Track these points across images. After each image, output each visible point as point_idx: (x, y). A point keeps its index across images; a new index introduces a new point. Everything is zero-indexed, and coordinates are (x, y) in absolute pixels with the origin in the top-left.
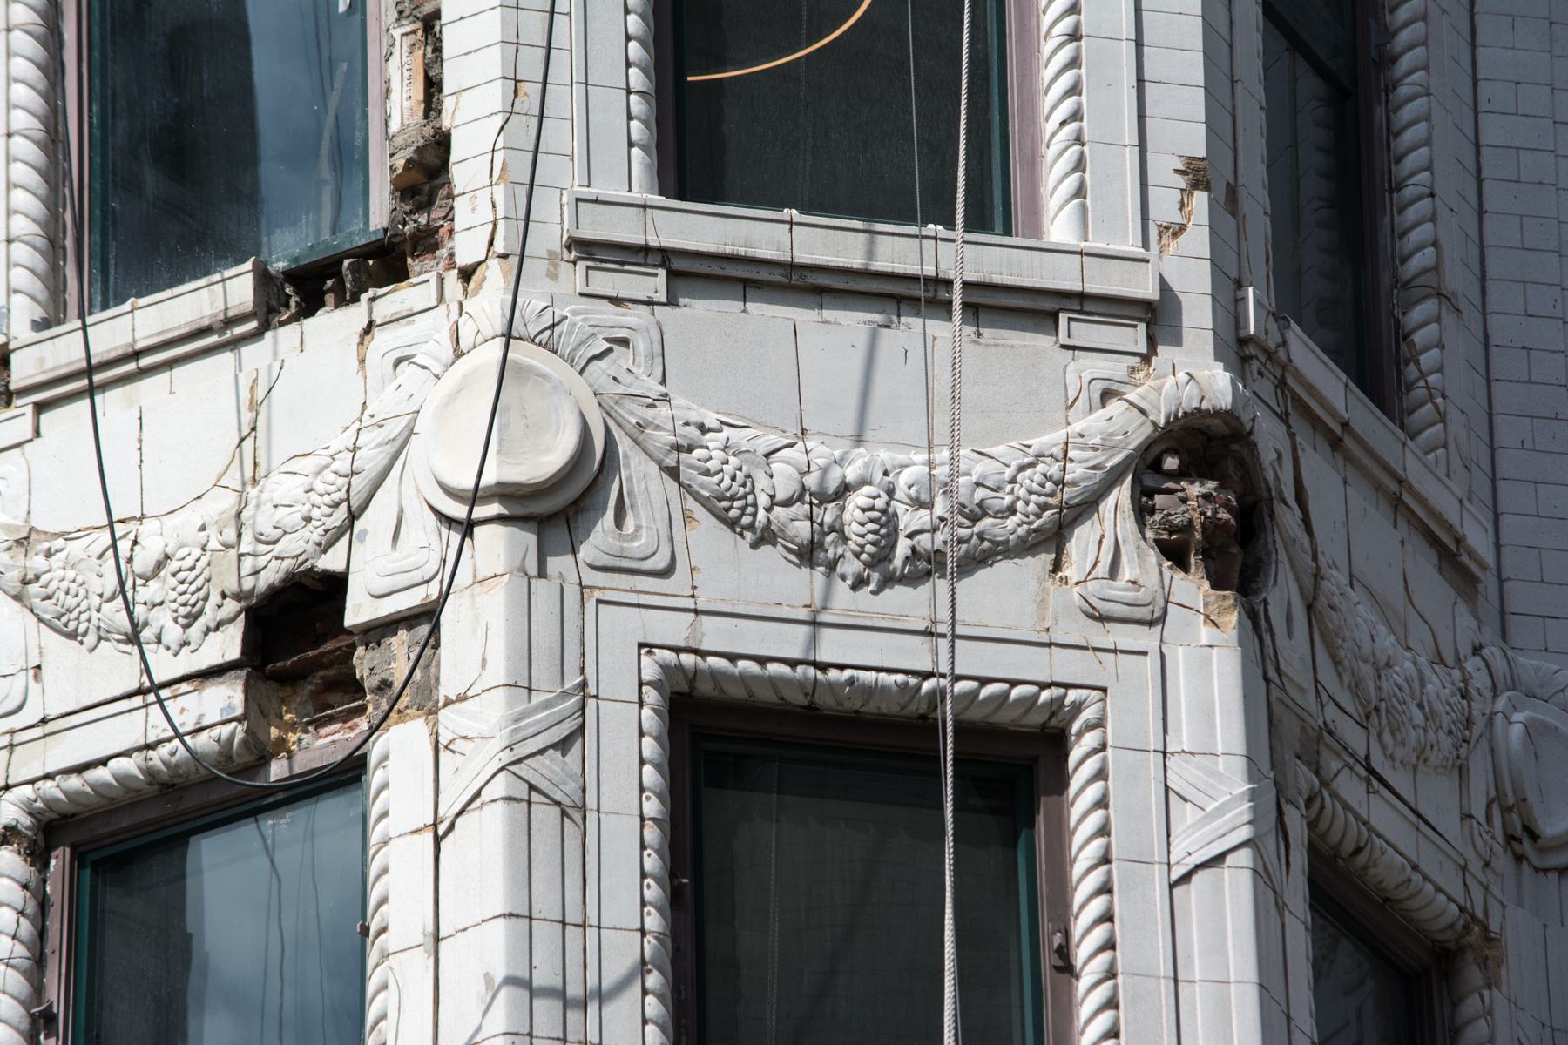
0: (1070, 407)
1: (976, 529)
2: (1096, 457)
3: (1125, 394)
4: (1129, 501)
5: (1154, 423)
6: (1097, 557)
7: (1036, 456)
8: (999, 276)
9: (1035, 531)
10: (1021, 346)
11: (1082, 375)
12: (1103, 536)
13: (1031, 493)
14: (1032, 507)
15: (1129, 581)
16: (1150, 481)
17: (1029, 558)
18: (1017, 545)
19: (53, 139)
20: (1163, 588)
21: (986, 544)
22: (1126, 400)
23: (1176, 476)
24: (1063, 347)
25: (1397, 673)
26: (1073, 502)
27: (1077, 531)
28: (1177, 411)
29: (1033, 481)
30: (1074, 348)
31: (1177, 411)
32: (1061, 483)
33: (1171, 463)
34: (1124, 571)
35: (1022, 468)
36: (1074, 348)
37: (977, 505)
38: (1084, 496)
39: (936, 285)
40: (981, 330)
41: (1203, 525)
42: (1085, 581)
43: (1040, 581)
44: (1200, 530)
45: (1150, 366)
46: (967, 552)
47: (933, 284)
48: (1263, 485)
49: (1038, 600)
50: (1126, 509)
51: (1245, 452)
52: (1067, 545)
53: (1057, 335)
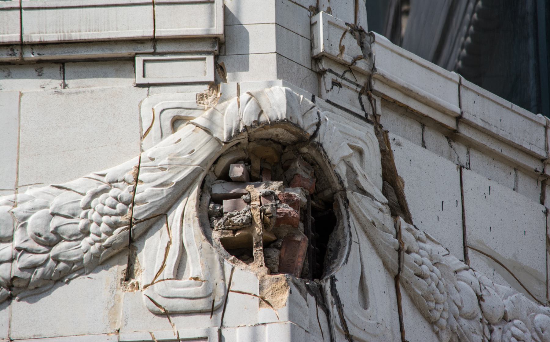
0: (142, 137)
1: (52, 254)
2: (163, 176)
3: (193, 118)
4: (194, 209)
5: (218, 140)
6: (164, 262)
7: (110, 183)
8: (78, 33)
9: (107, 247)
10: (100, 90)
11: (155, 107)
12: (170, 243)
13: (102, 215)
14: (104, 227)
15: (192, 278)
16: (218, 189)
17: (103, 271)
18: (90, 262)
19: (12, 42)
20: (224, 280)
21: (62, 265)
22: (193, 124)
23: (239, 182)
24: (139, 86)
25: (516, 326)
26: (141, 217)
27: (147, 242)
28: (239, 126)
29: (104, 205)
30: (148, 85)
31: (239, 126)
32: (132, 202)
33: (238, 171)
34: (189, 270)
35: (95, 195)
36: (148, 85)
37: (52, 232)
38: (151, 211)
39: (22, 49)
40: (67, 82)
41: (263, 220)
42: (152, 283)
43: (112, 290)
44: (260, 226)
45: (218, 91)
46: (43, 274)
47: (19, 48)
48: (335, 179)
49: (110, 307)
50: (191, 217)
51: (314, 152)
52: (138, 255)
53: (135, 78)
